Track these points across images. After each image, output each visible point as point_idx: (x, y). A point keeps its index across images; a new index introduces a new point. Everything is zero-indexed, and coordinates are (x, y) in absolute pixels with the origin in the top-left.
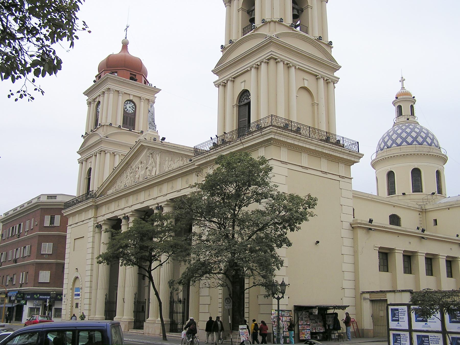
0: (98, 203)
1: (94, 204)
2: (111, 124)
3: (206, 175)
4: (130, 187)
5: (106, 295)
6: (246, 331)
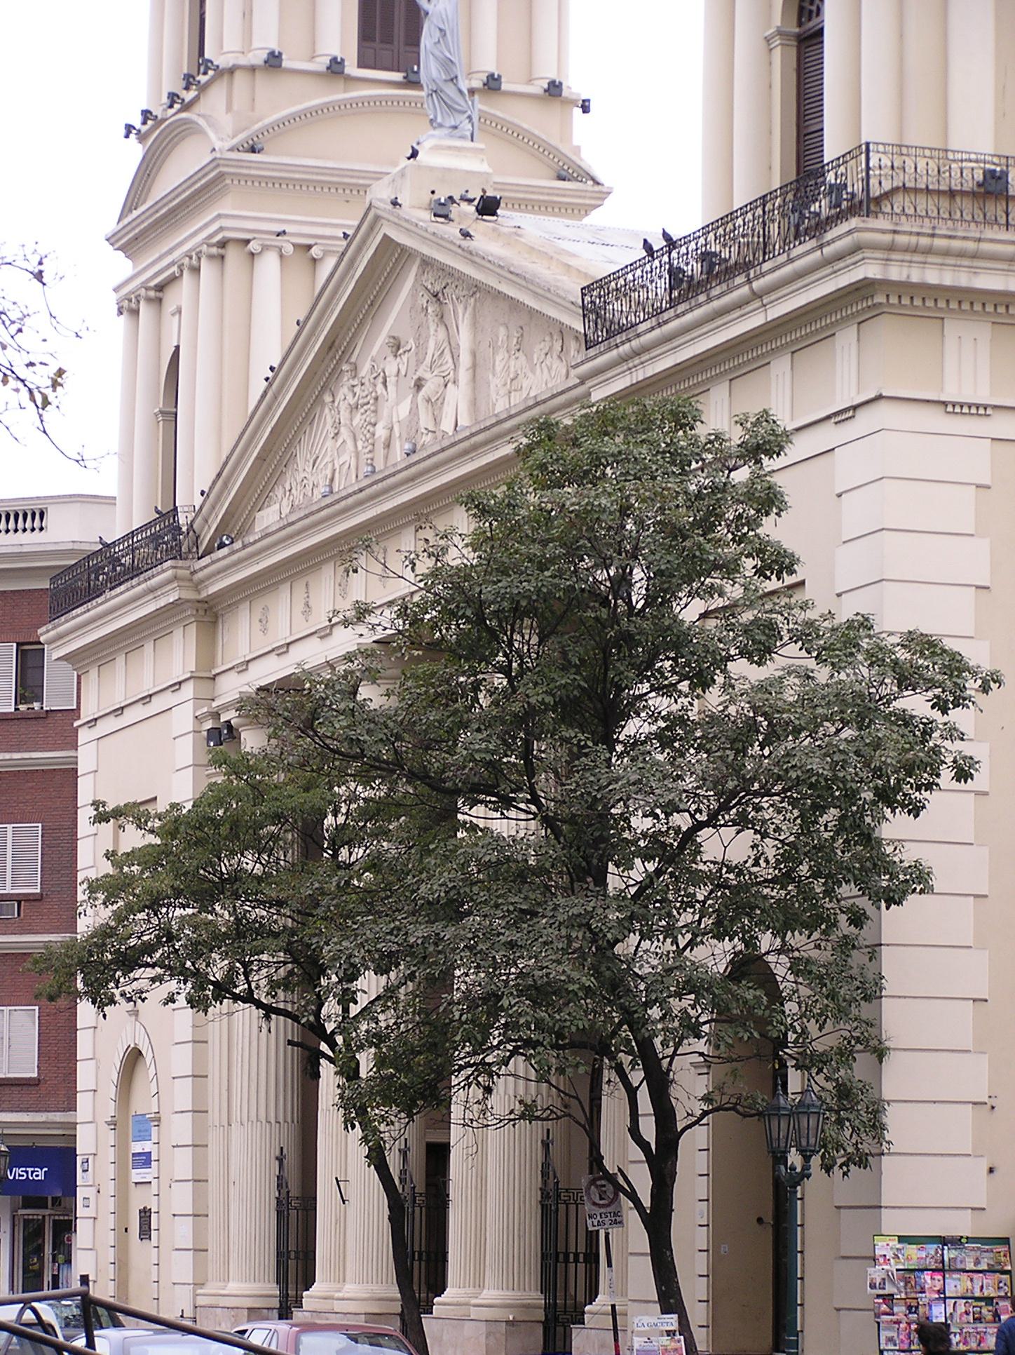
0: (213, 589)
1: (189, 595)
2: (274, 61)
3: (754, 410)
4: (394, 474)
5: (280, 1160)
6: (674, 1345)
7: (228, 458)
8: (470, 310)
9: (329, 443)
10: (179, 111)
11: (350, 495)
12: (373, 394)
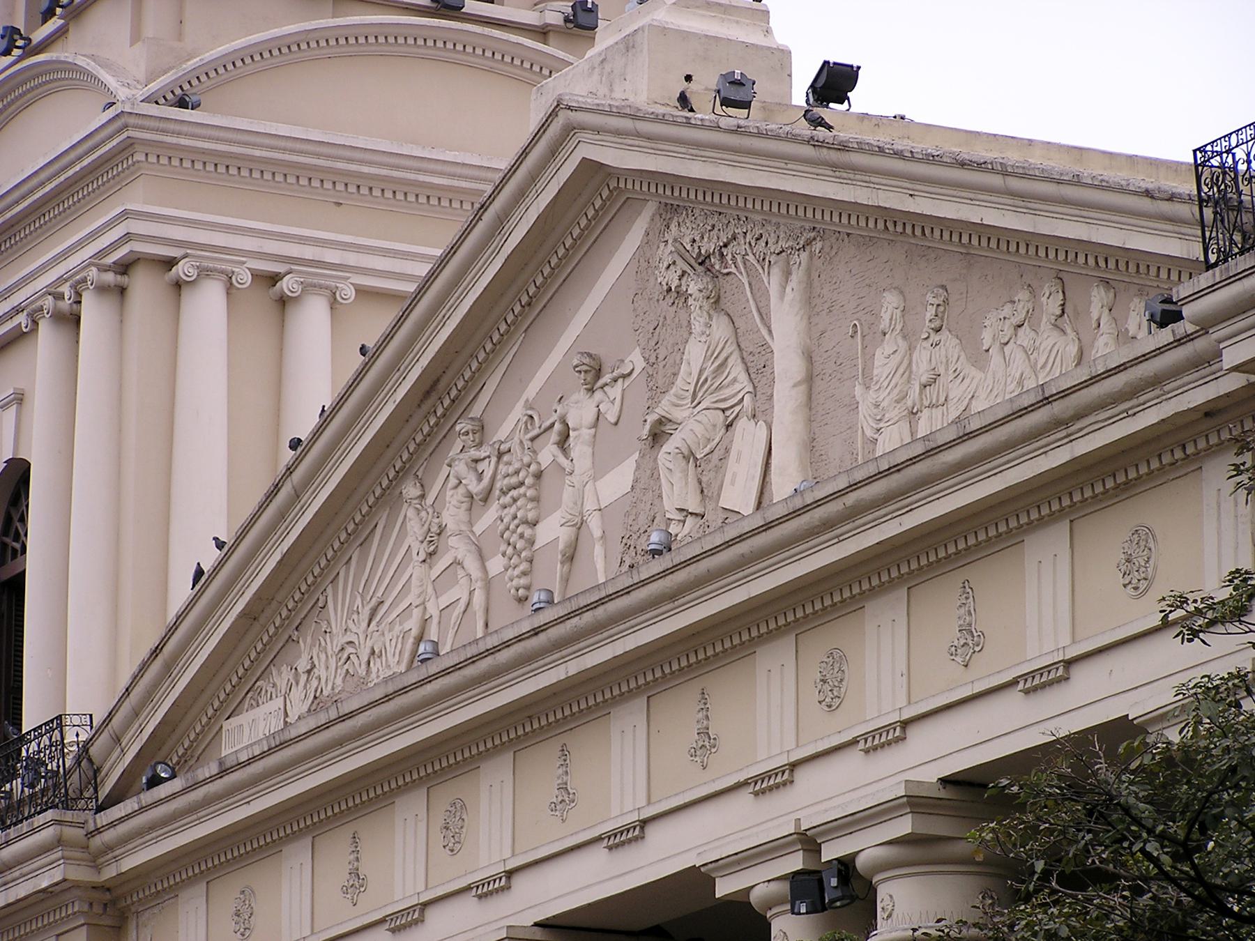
0: (128, 864)
1: (80, 874)
7: (180, 617)
8: (797, 277)
9: (415, 570)
10: (20, 59)
11: (507, 644)
12: (533, 468)
